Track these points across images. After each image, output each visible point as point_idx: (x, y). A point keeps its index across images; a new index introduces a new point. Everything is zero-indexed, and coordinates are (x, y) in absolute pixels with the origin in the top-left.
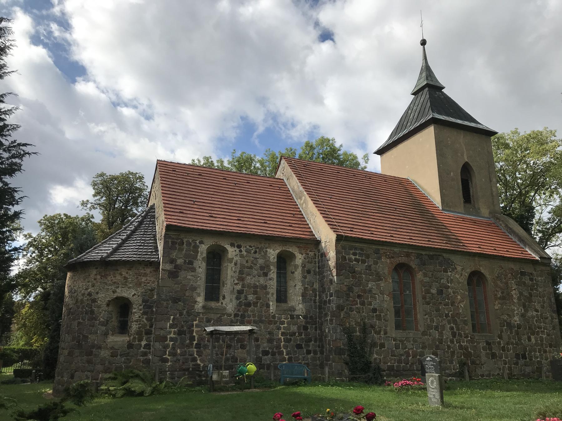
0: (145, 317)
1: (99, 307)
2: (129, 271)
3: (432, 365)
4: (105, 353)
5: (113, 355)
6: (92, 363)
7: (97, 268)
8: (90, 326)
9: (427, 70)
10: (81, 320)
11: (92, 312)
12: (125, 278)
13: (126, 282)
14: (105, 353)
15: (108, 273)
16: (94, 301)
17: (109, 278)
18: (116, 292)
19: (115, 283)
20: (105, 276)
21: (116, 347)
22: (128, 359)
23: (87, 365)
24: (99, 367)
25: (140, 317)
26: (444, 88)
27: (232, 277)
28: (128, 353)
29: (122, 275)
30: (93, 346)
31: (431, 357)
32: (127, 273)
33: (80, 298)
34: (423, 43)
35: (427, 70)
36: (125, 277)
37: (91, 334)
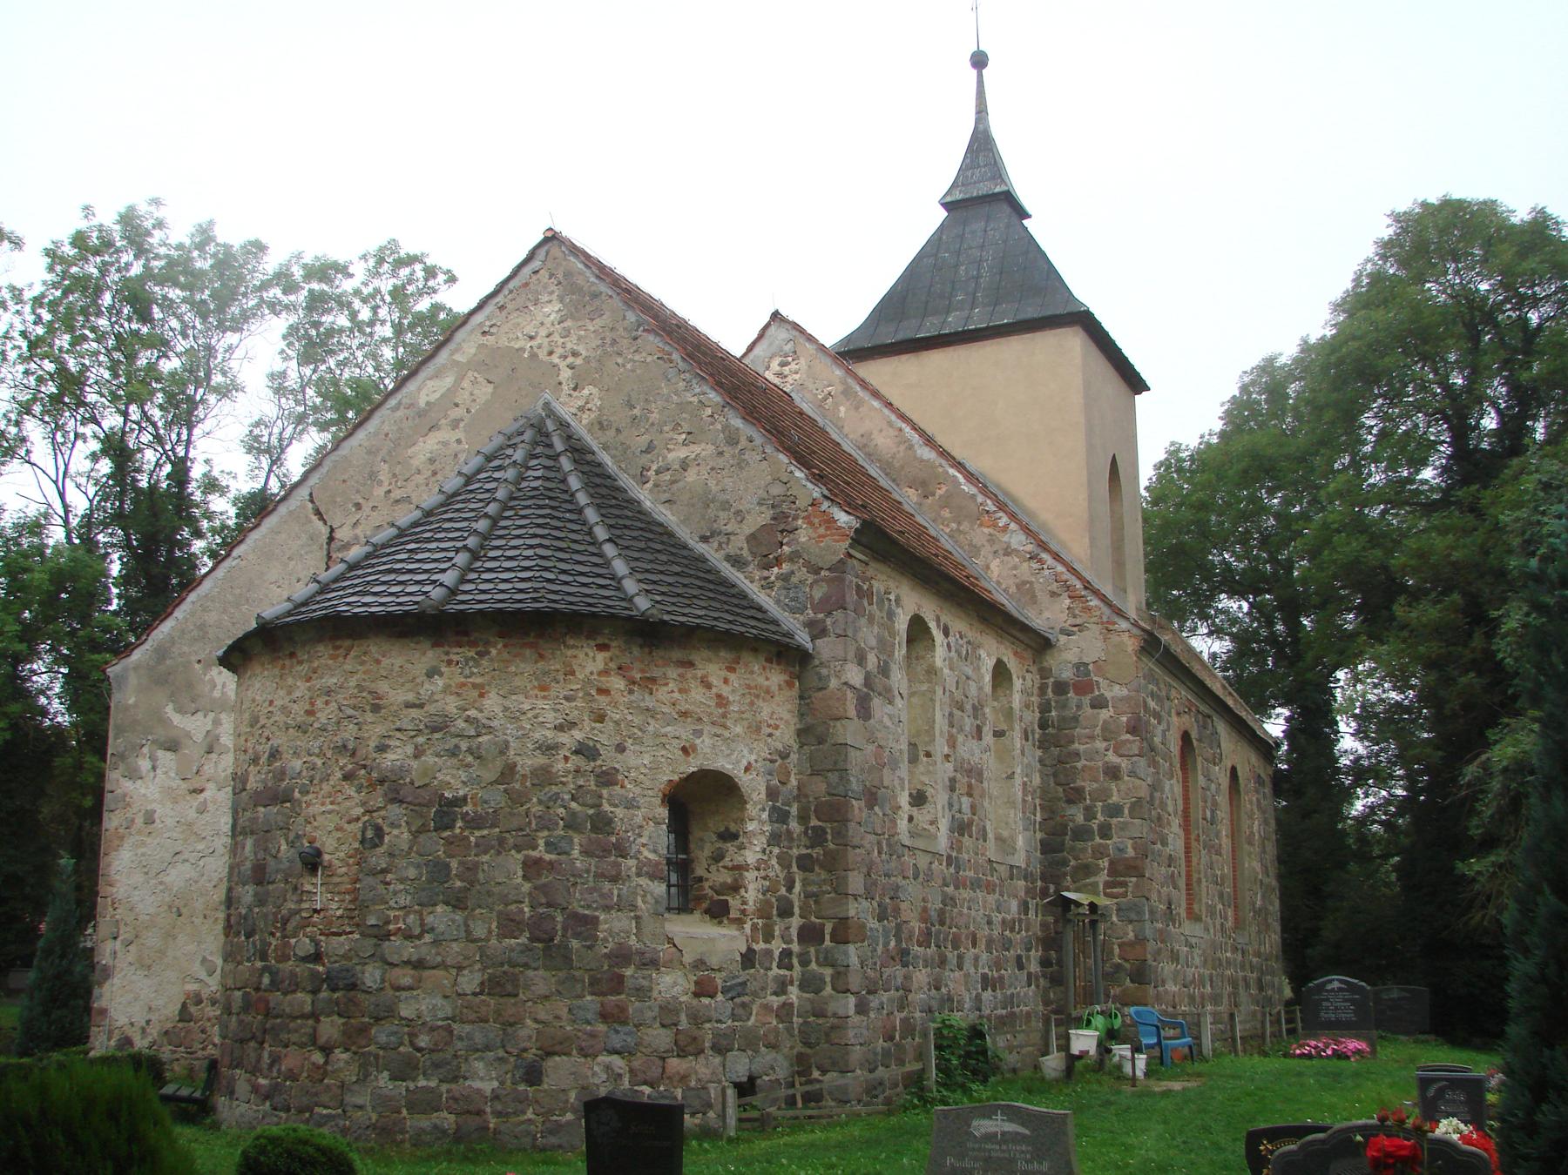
0: (776, 850)
1: (631, 805)
2: (732, 677)
3: (1345, 1000)
4: (672, 985)
5: (703, 989)
6: (624, 1023)
7: (602, 647)
8: (600, 876)
9: (982, 147)
10: (540, 852)
11: (602, 823)
12: (721, 701)
13: (724, 716)
14: (672, 985)
15: (656, 672)
16: (608, 778)
17: (662, 693)
18: (694, 748)
19: (684, 714)
20: (649, 683)
21: (714, 961)
22: (744, 1005)
23: (602, 1027)
24: (660, 1038)
25: (764, 851)
26: (1029, 216)
27: (1367, 795)
28: (744, 984)
29: (709, 686)
30: (622, 956)
31: (1341, 981)
32: (726, 681)
33: (527, 762)
34: (979, 61)
35: (982, 147)
36: (719, 696)
37: (607, 908)
